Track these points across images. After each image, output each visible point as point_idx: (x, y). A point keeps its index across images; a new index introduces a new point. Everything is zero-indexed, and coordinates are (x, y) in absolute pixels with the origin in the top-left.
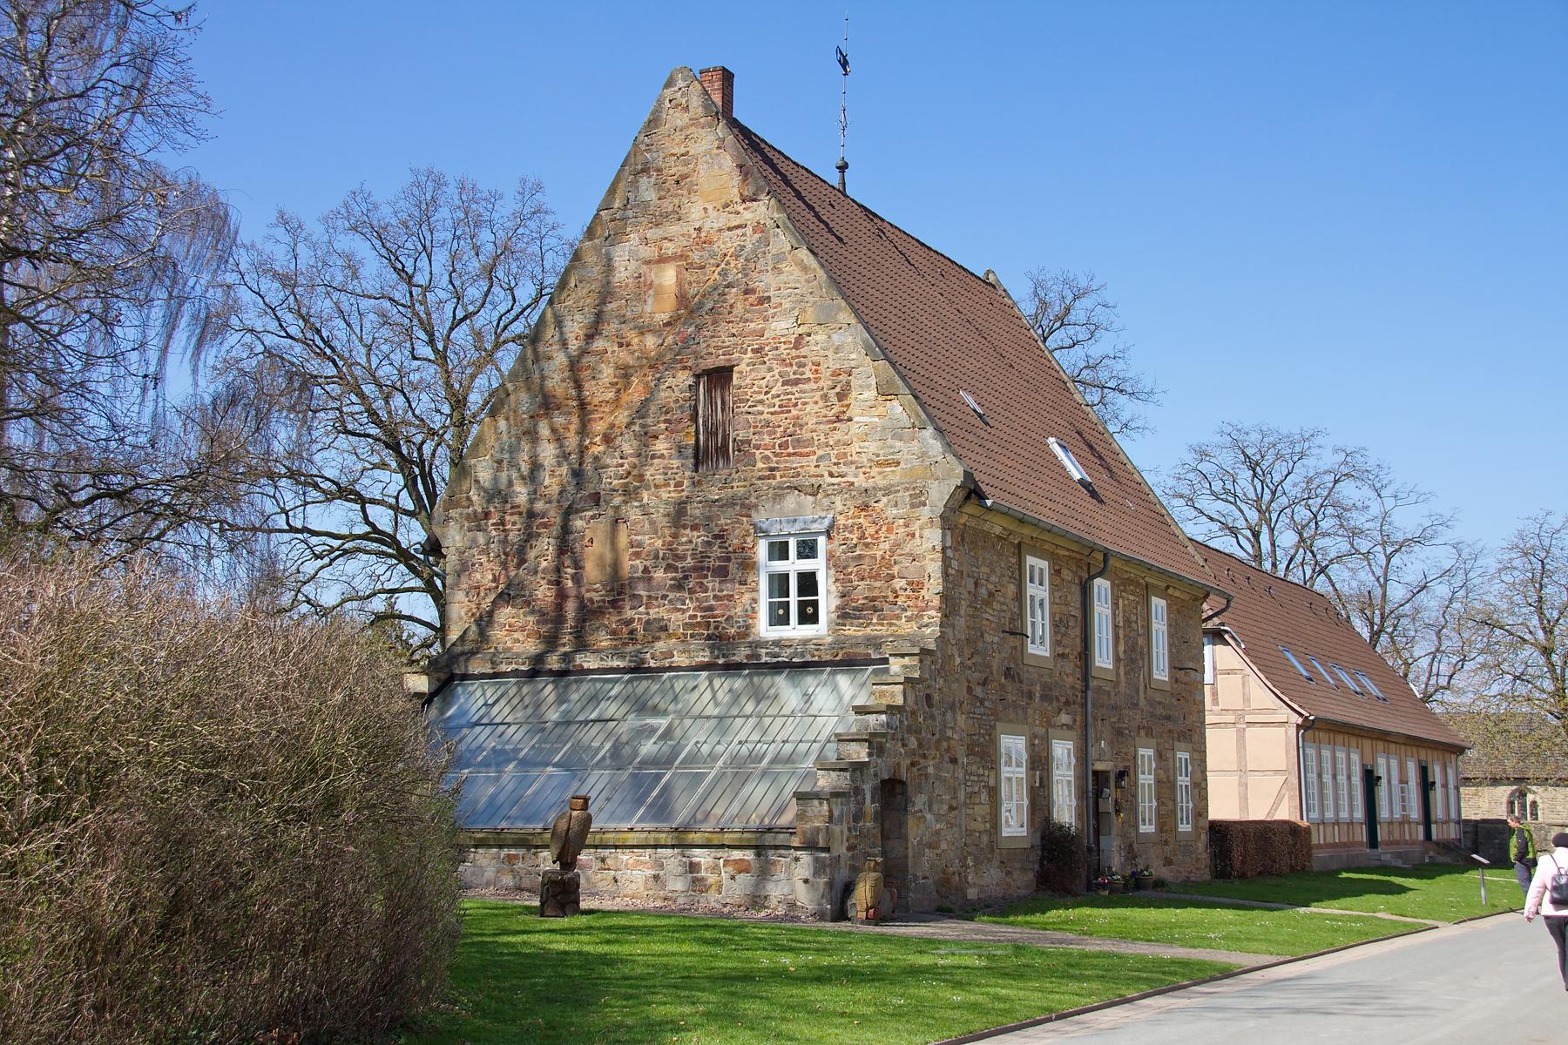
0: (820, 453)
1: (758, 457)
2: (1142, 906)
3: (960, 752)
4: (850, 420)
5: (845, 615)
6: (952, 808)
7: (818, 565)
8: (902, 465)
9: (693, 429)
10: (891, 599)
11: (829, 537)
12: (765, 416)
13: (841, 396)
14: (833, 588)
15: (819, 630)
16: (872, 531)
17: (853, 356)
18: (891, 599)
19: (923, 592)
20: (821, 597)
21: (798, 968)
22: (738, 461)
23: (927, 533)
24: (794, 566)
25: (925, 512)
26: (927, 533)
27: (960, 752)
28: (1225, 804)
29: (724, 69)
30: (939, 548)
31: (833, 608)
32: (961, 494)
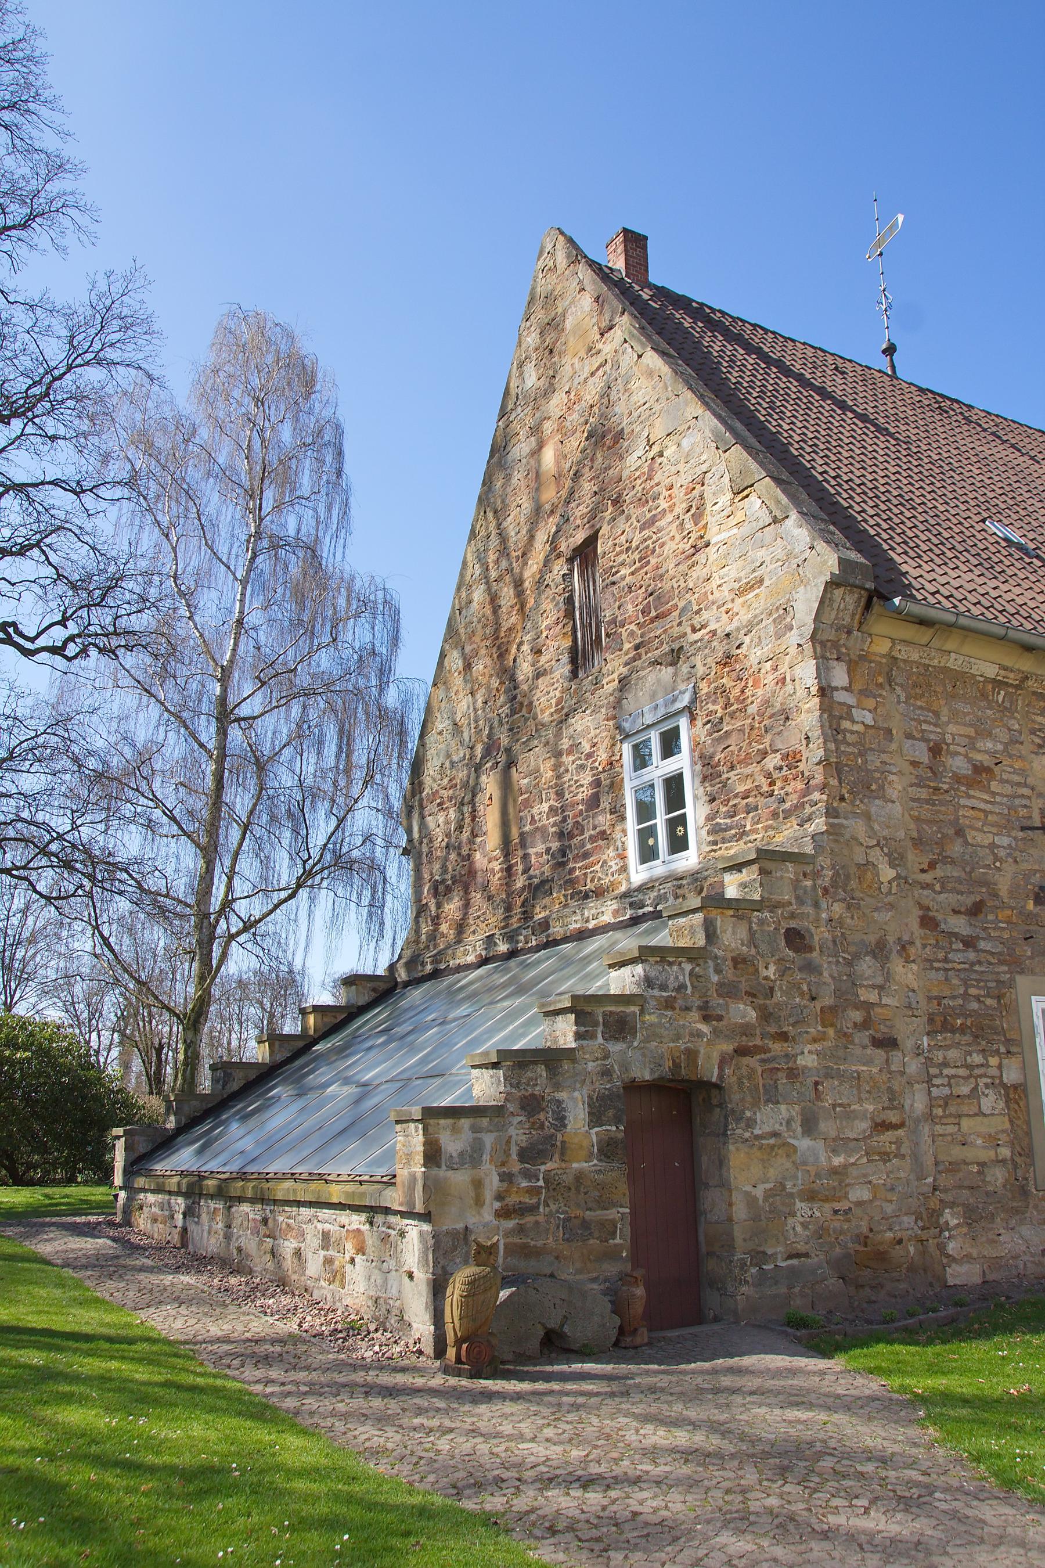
0: (681, 605)
1: (624, 635)
2: (984, 1333)
3: (911, 1032)
4: (707, 545)
5: (716, 832)
6: (882, 1126)
7: (682, 762)
8: (767, 583)
9: (569, 628)
10: (765, 788)
11: (693, 719)
12: (628, 579)
13: (697, 517)
14: (701, 791)
15: (689, 860)
16: (736, 692)
17: (704, 457)
18: (765, 788)
19: (802, 766)
20: (689, 810)
21: (925, 1389)
22: (608, 648)
23: (798, 671)
24: (660, 768)
25: (793, 638)
26: (798, 671)
27: (911, 1032)
28: (728, 896)
29: (625, 231)
30: (814, 690)
31: (702, 820)
32: (848, 601)
